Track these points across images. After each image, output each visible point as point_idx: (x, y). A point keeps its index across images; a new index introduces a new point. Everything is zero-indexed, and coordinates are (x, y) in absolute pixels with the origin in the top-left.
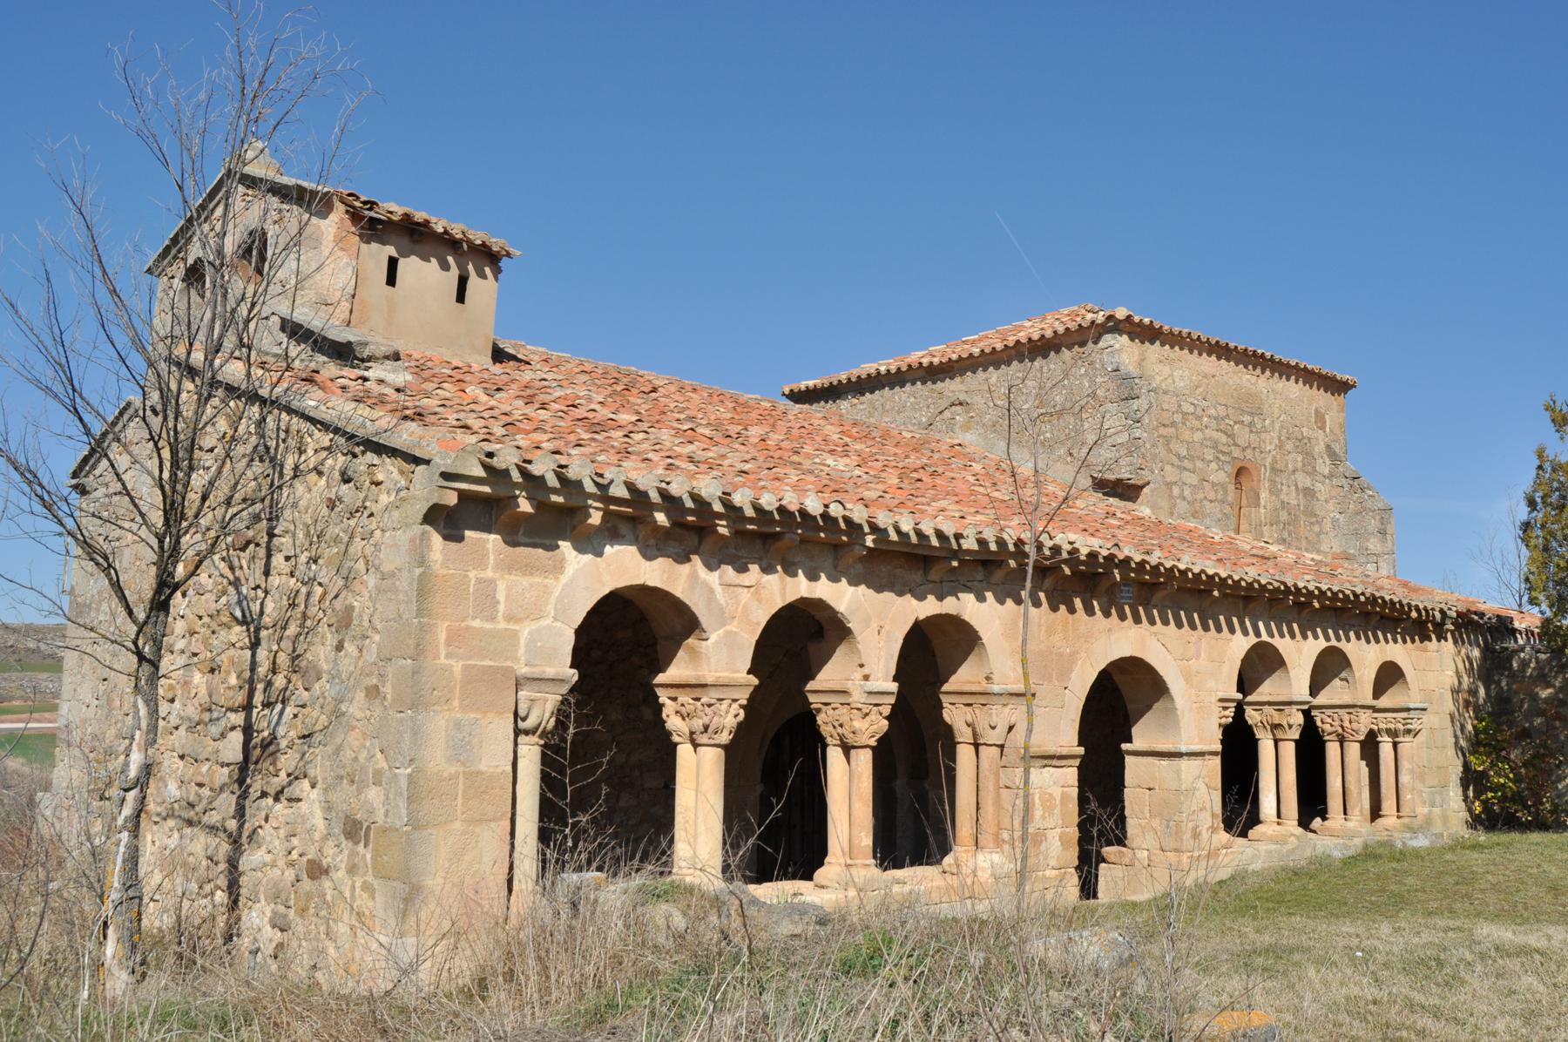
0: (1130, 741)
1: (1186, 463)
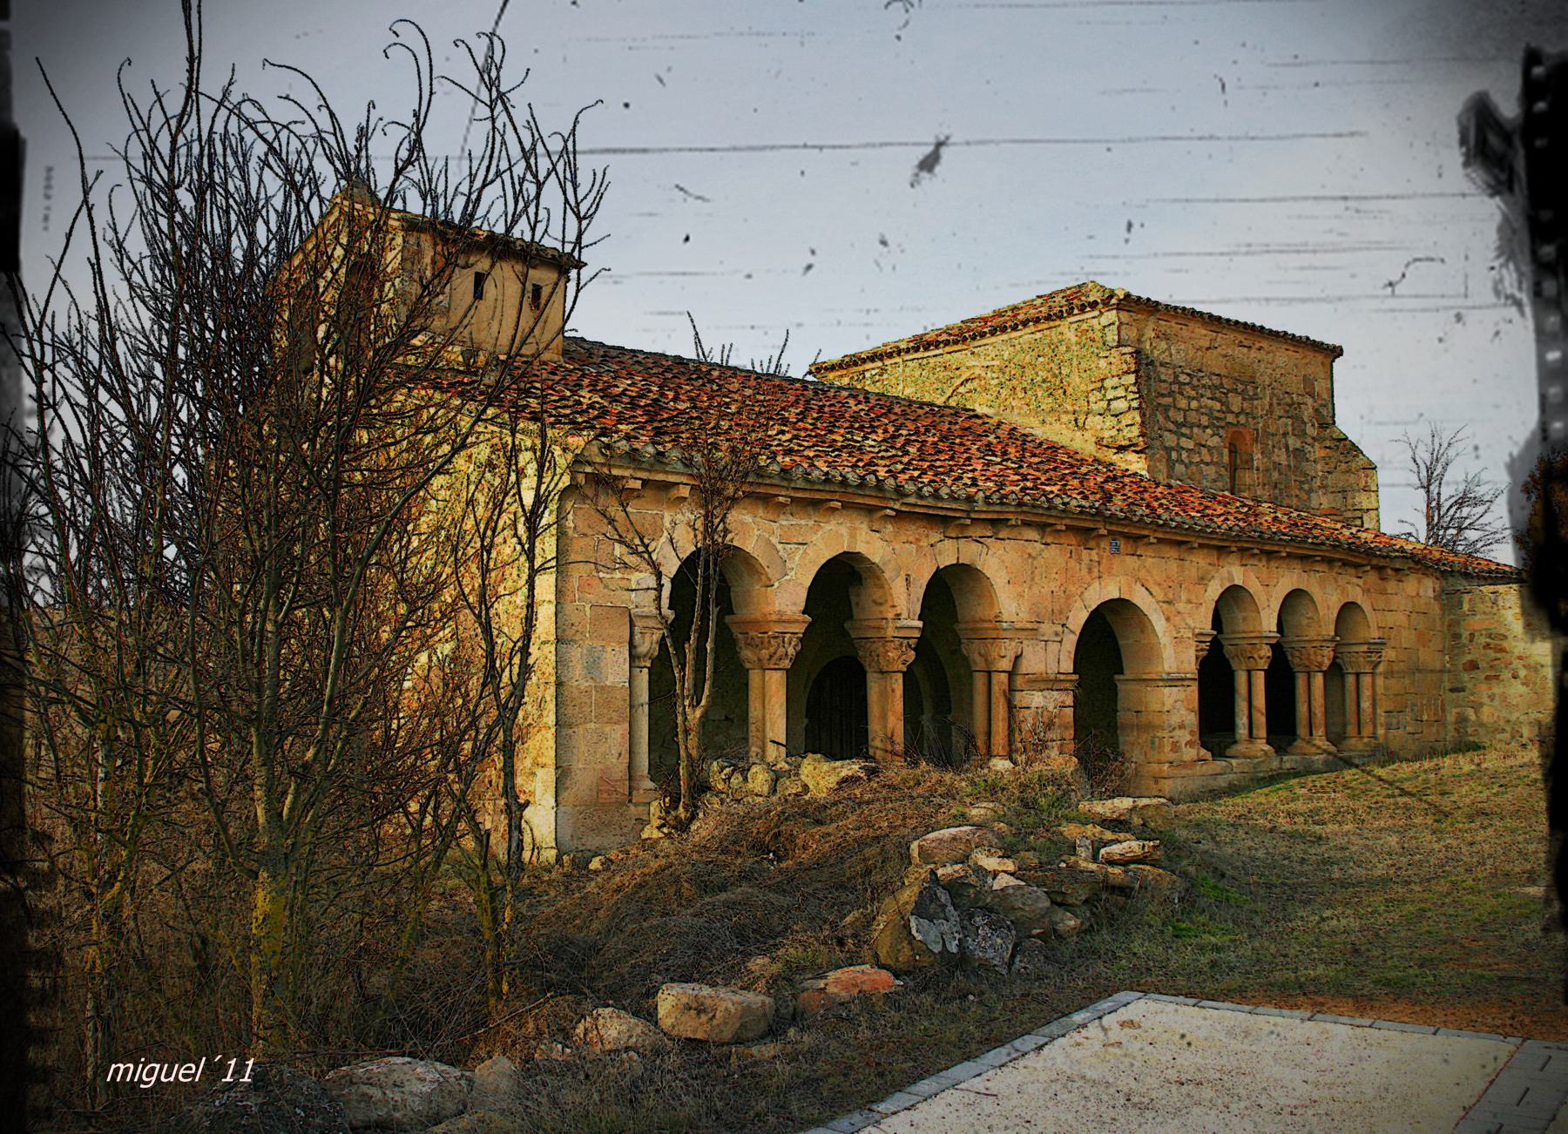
0: (1122, 673)
1: (1184, 430)
